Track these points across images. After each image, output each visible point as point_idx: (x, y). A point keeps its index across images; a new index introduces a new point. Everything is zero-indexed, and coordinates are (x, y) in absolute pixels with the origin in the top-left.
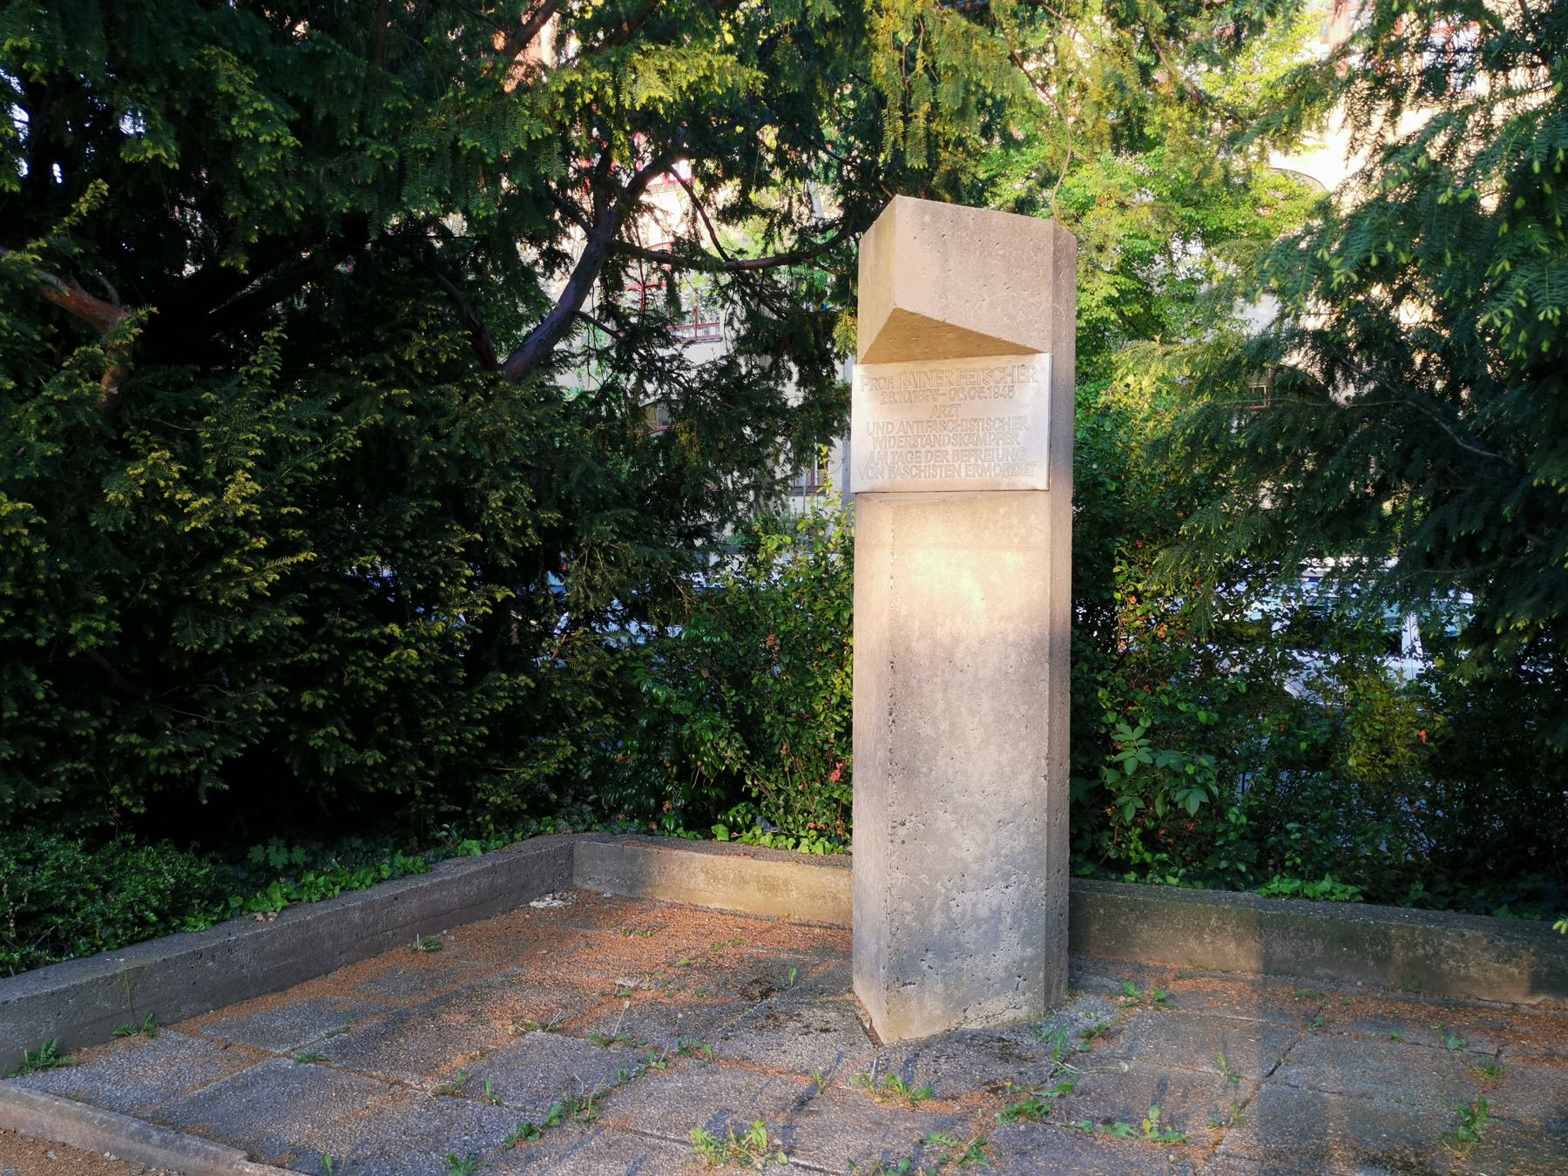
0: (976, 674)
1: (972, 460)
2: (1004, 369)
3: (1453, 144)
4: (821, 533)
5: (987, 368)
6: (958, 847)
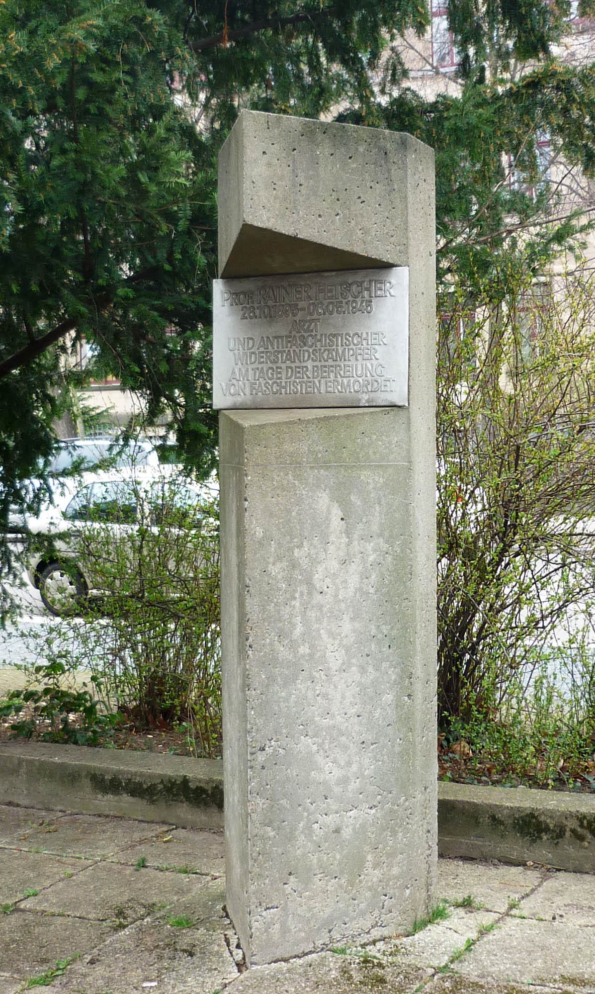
0: (336, 596)
1: (332, 375)
4: (458, 265)
6: (320, 770)
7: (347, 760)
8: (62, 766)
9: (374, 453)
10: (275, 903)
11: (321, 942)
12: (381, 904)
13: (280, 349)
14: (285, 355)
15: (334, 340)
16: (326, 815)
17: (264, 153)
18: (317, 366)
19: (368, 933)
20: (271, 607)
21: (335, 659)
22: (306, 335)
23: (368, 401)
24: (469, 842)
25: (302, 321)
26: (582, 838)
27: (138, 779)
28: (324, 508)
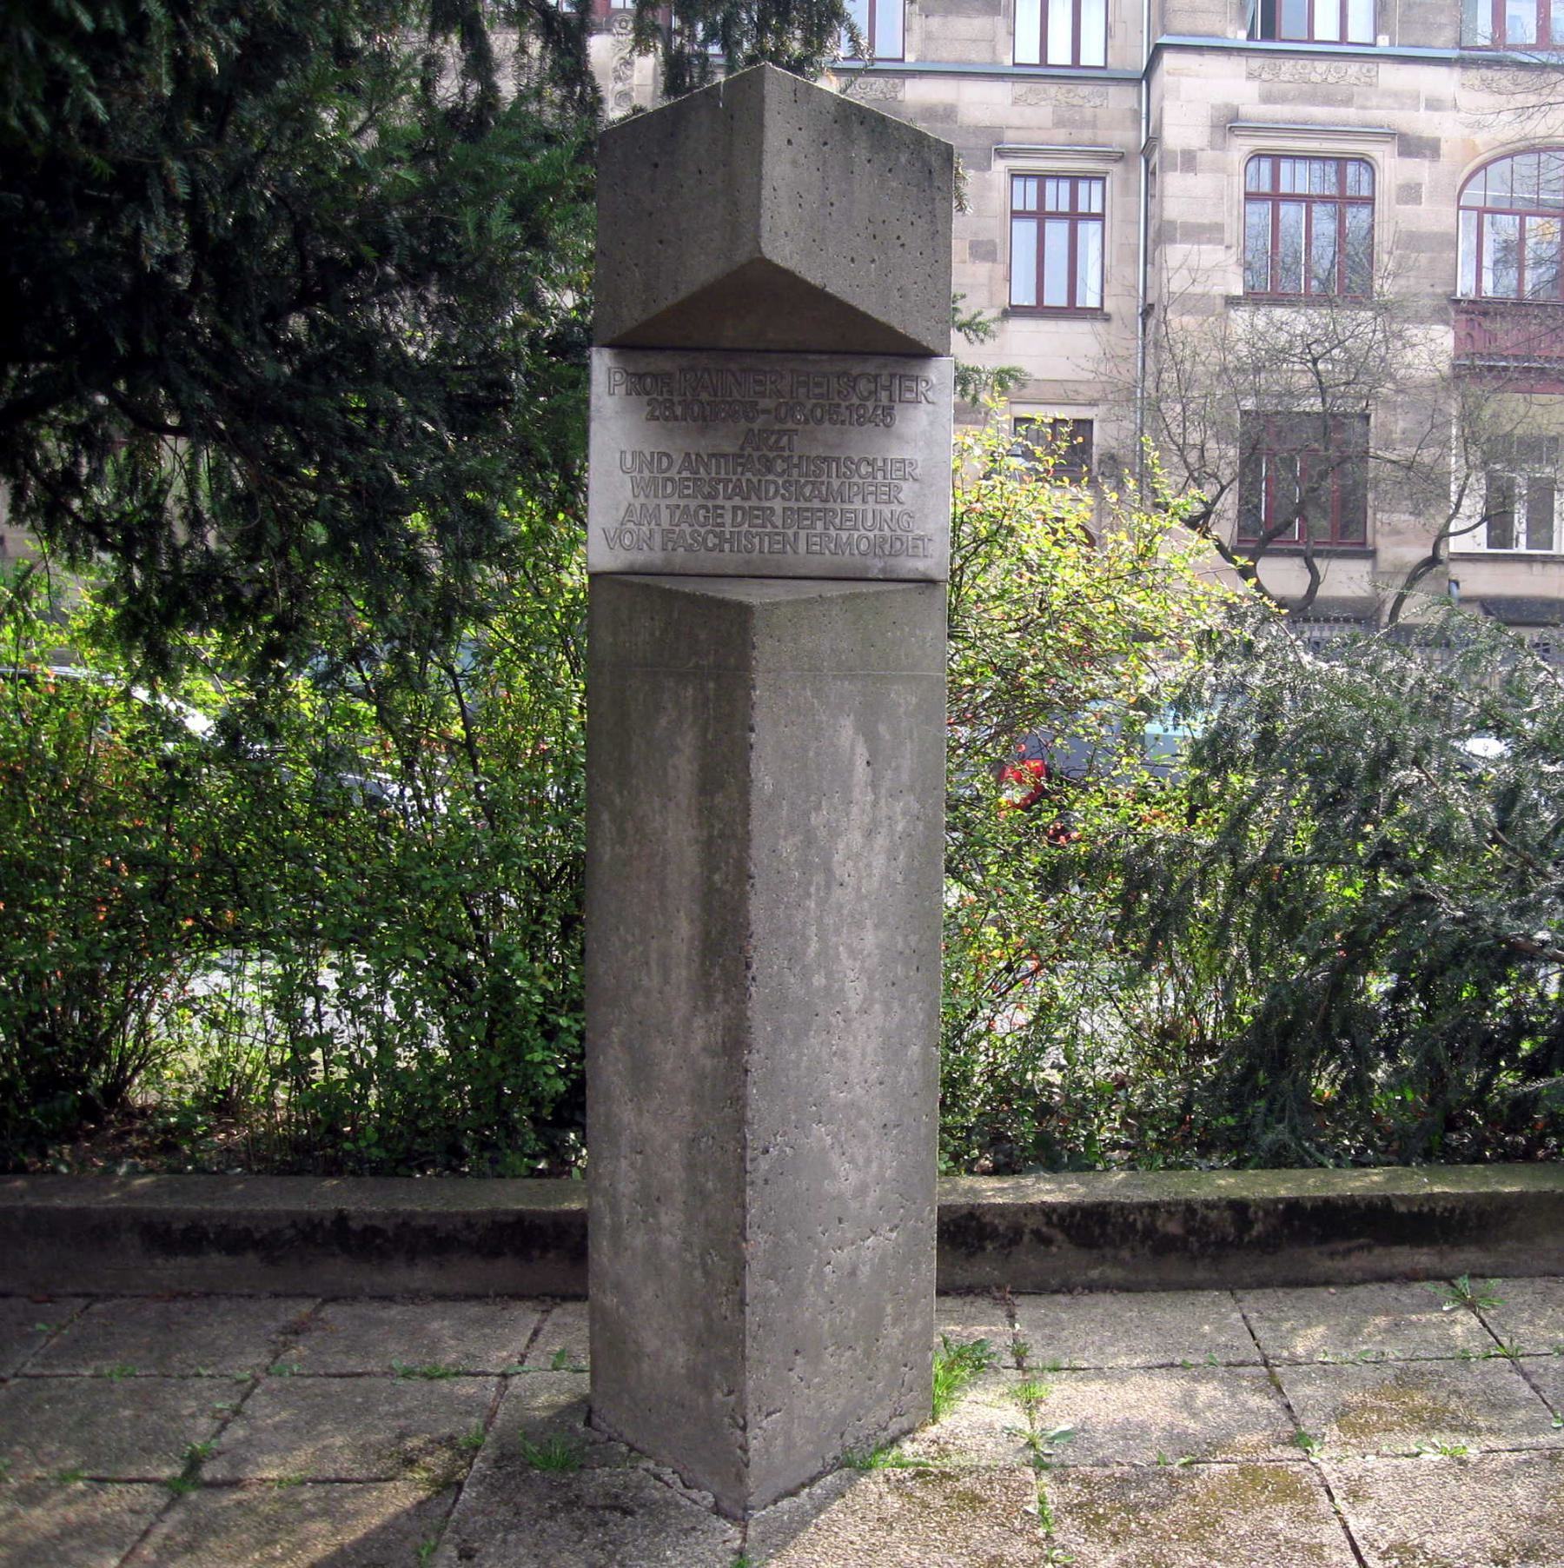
1: (819, 524)
2: (876, 377)
3: (737, 1283)
5: (845, 374)
6: (834, 1176)
8: (80, 1214)
9: (907, 656)
10: (778, 1404)
11: (831, 1455)
13: (723, 476)
15: (825, 466)
17: (789, 142)
18: (790, 509)
19: (885, 1429)
20: (780, 912)
21: (855, 991)
22: (771, 455)
23: (883, 570)
24: (985, 1269)
25: (765, 431)
26: (1047, 1241)
27: (242, 1224)
28: (847, 744)
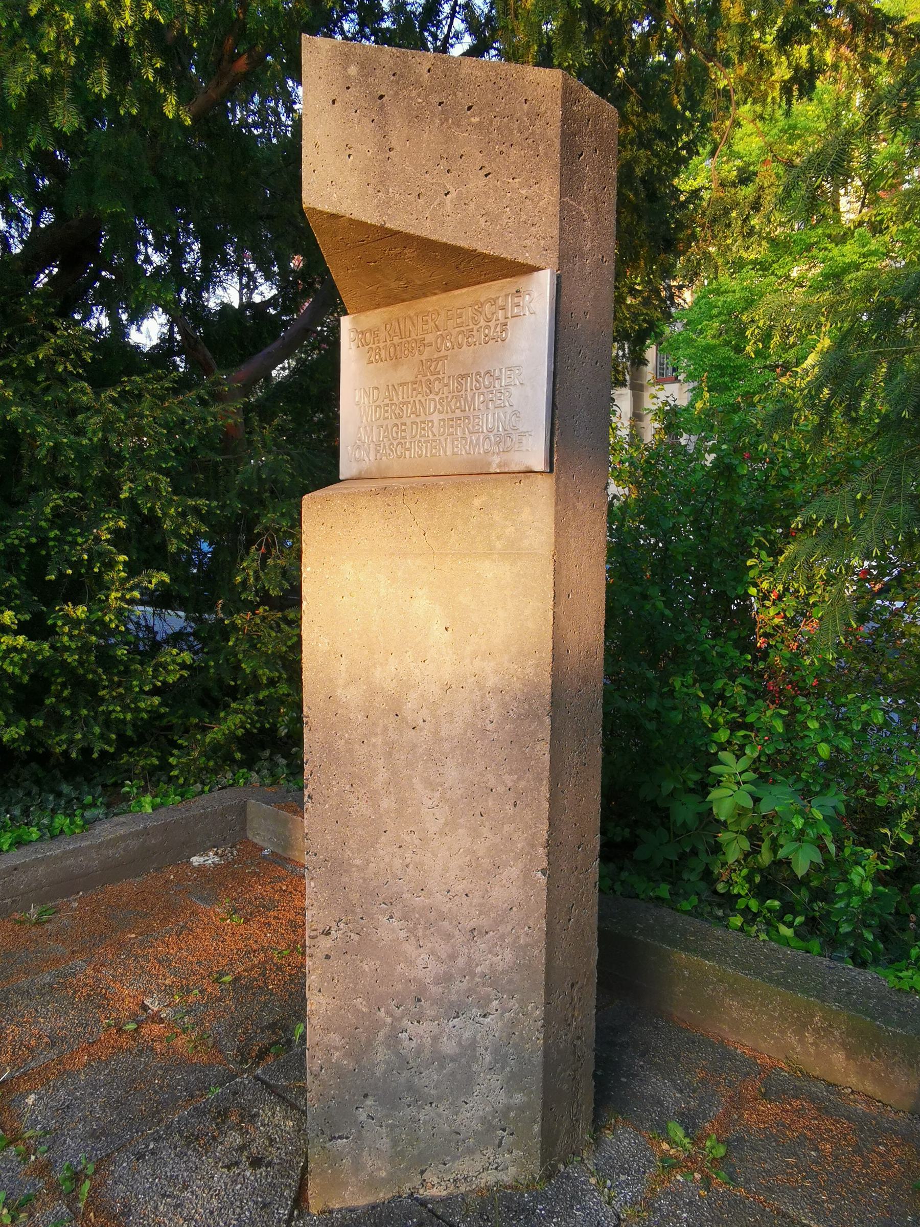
7: (450, 951)
12: (497, 1142)
14: (410, 406)
16: (419, 1022)
22: (432, 378)
23: (499, 466)
